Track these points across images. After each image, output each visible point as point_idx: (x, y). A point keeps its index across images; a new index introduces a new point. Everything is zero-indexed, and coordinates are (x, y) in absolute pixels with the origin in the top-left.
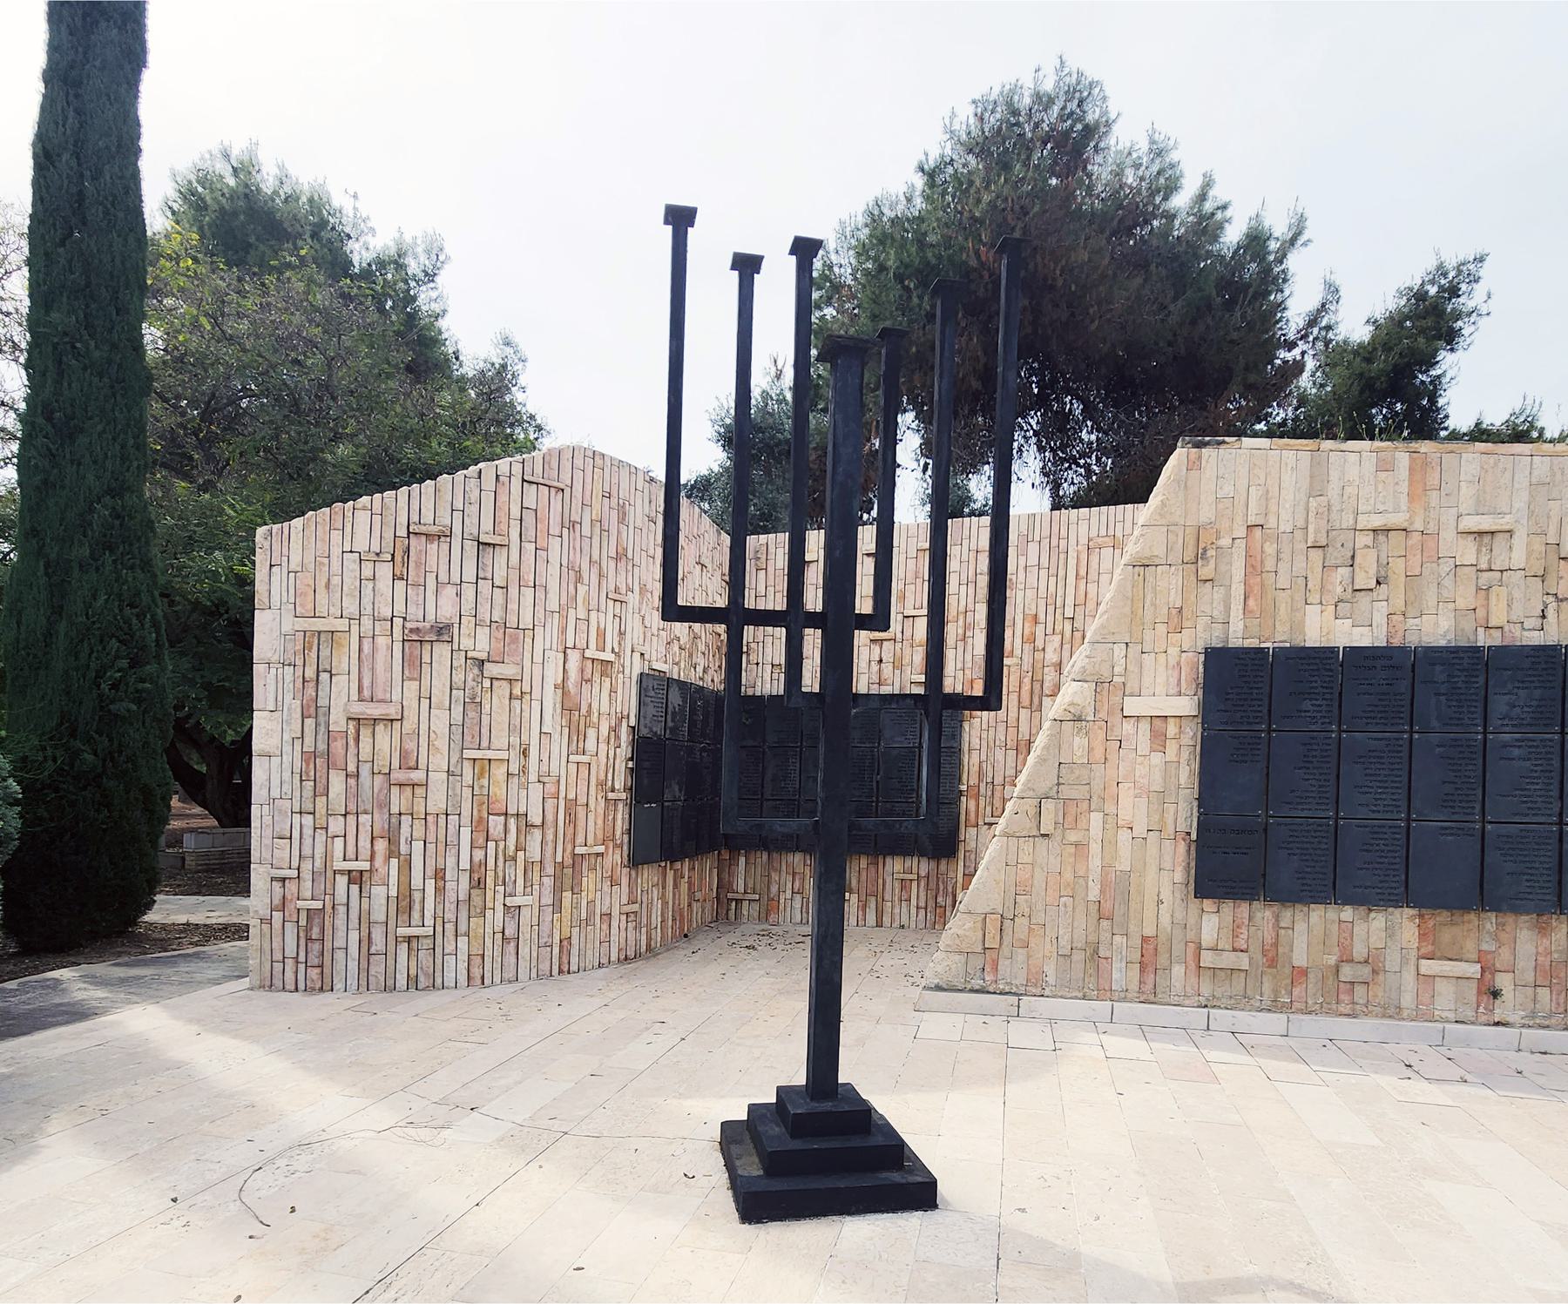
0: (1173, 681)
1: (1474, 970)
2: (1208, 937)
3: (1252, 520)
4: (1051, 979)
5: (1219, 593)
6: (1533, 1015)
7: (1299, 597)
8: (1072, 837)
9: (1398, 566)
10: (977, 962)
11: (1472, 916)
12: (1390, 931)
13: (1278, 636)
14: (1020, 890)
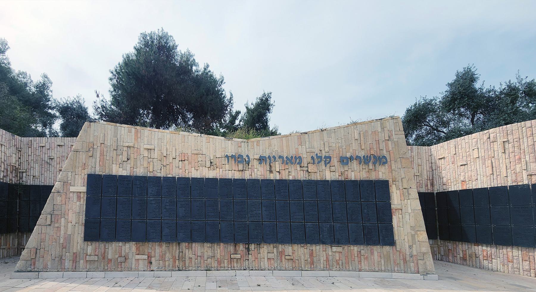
0: (82, 182)
1: (146, 257)
2: (89, 252)
3: (101, 142)
4: (49, 267)
5: (94, 160)
6: (159, 268)
7: (111, 162)
8: (56, 225)
9: (132, 156)
10: (29, 263)
11: (146, 243)
12: (130, 248)
13: (106, 172)
14: (42, 241)
